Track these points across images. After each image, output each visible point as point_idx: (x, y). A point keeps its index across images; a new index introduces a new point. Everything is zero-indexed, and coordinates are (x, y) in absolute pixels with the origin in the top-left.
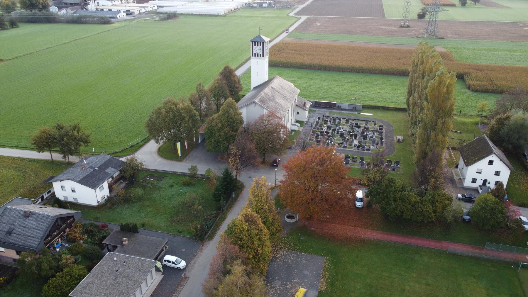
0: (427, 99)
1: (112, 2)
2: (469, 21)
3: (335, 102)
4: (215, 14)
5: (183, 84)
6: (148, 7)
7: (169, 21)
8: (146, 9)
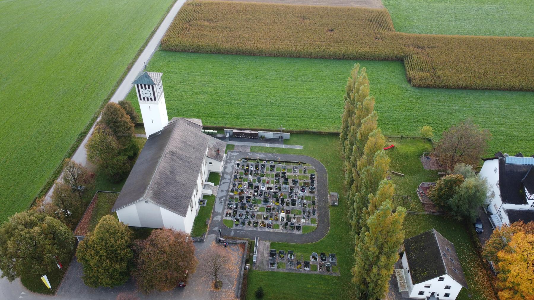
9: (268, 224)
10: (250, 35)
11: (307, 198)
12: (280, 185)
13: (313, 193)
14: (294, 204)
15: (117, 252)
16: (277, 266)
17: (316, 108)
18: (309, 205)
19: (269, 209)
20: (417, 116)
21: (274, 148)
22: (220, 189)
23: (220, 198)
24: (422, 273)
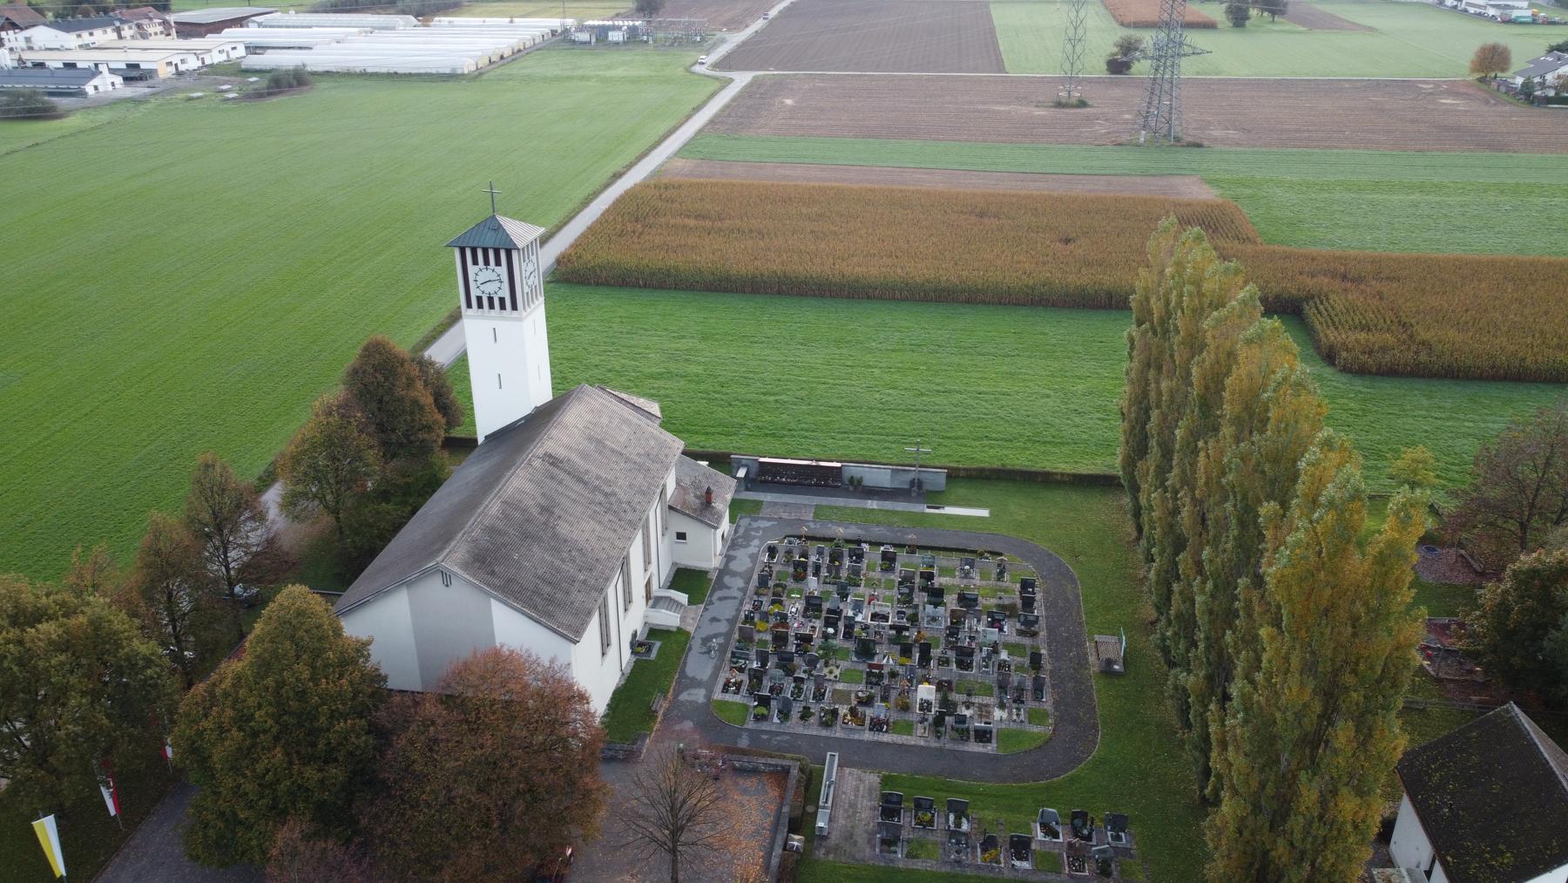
0: (1277, 623)
1: (79, 36)
2: (1267, 80)
3: (839, 465)
4: (441, 71)
5: (241, 385)
6: (209, 51)
7: (275, 100)
8: (203, 59)
9: (872, 719)
10: (823, 246)
11: (1013, 648)
12: (916, 606)
13: (1034, 635)
14: (964, 664)
15: (316, 725)
16: (905, 851)
17: (1028, 416)
18: (1020, 668)
19: (874, 677)
20: (1369, 443)
21: (895, 513)
22: (708, 615)
23: (706, 640)
24: (1492, 858)
